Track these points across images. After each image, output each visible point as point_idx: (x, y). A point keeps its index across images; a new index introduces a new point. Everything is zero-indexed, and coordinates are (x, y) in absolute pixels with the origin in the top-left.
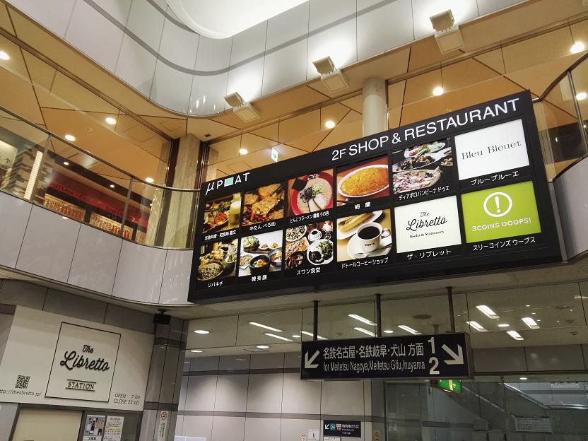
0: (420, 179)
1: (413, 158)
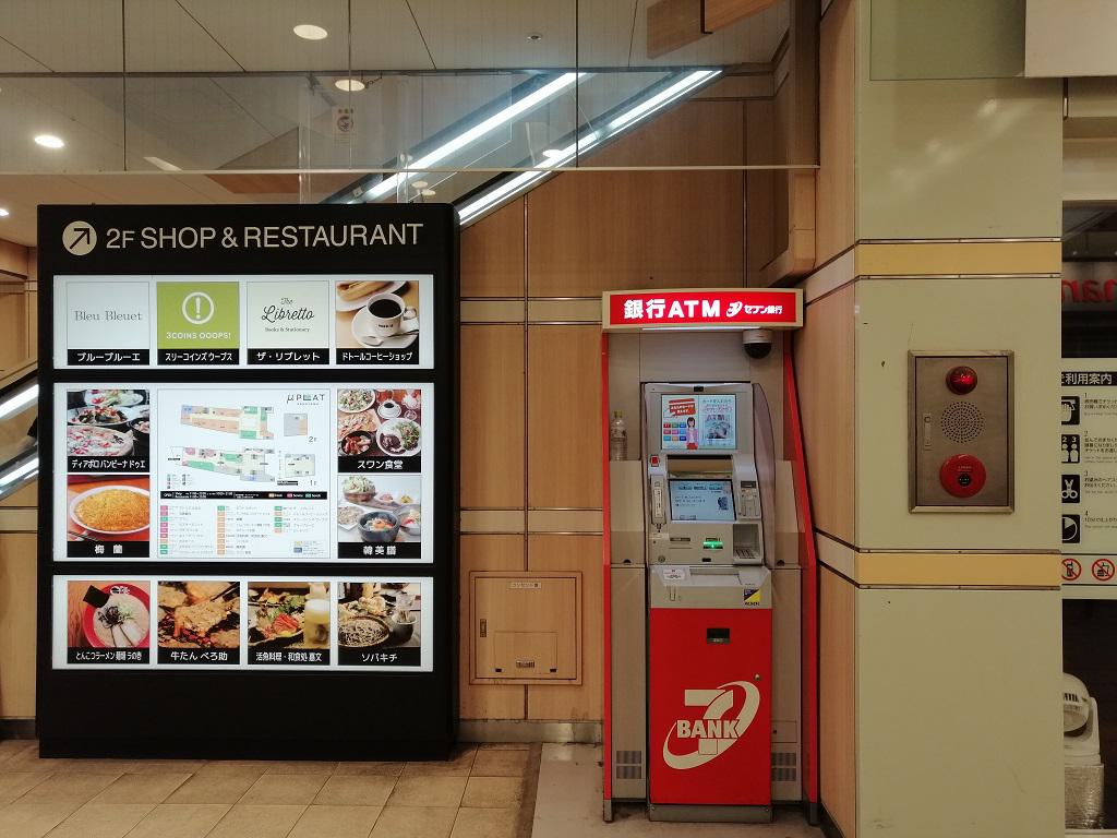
0: (105, 442)
1: (97, 408)
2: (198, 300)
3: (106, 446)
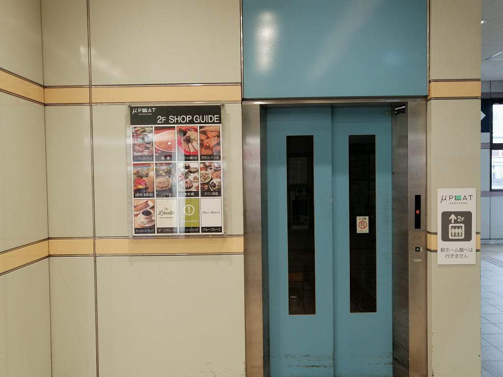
0: (141, 149)
2: (189, 207)
3: (142, 151)
